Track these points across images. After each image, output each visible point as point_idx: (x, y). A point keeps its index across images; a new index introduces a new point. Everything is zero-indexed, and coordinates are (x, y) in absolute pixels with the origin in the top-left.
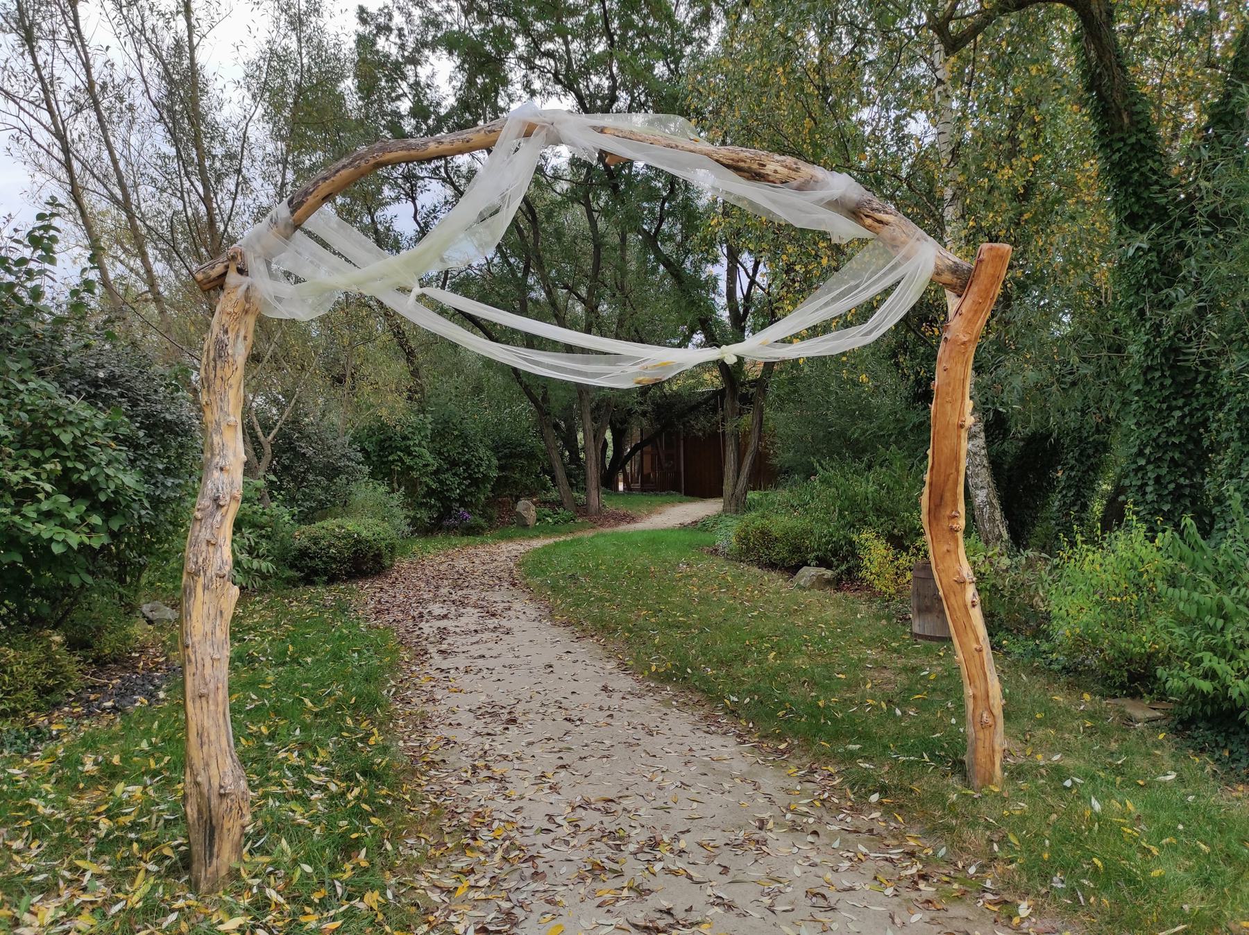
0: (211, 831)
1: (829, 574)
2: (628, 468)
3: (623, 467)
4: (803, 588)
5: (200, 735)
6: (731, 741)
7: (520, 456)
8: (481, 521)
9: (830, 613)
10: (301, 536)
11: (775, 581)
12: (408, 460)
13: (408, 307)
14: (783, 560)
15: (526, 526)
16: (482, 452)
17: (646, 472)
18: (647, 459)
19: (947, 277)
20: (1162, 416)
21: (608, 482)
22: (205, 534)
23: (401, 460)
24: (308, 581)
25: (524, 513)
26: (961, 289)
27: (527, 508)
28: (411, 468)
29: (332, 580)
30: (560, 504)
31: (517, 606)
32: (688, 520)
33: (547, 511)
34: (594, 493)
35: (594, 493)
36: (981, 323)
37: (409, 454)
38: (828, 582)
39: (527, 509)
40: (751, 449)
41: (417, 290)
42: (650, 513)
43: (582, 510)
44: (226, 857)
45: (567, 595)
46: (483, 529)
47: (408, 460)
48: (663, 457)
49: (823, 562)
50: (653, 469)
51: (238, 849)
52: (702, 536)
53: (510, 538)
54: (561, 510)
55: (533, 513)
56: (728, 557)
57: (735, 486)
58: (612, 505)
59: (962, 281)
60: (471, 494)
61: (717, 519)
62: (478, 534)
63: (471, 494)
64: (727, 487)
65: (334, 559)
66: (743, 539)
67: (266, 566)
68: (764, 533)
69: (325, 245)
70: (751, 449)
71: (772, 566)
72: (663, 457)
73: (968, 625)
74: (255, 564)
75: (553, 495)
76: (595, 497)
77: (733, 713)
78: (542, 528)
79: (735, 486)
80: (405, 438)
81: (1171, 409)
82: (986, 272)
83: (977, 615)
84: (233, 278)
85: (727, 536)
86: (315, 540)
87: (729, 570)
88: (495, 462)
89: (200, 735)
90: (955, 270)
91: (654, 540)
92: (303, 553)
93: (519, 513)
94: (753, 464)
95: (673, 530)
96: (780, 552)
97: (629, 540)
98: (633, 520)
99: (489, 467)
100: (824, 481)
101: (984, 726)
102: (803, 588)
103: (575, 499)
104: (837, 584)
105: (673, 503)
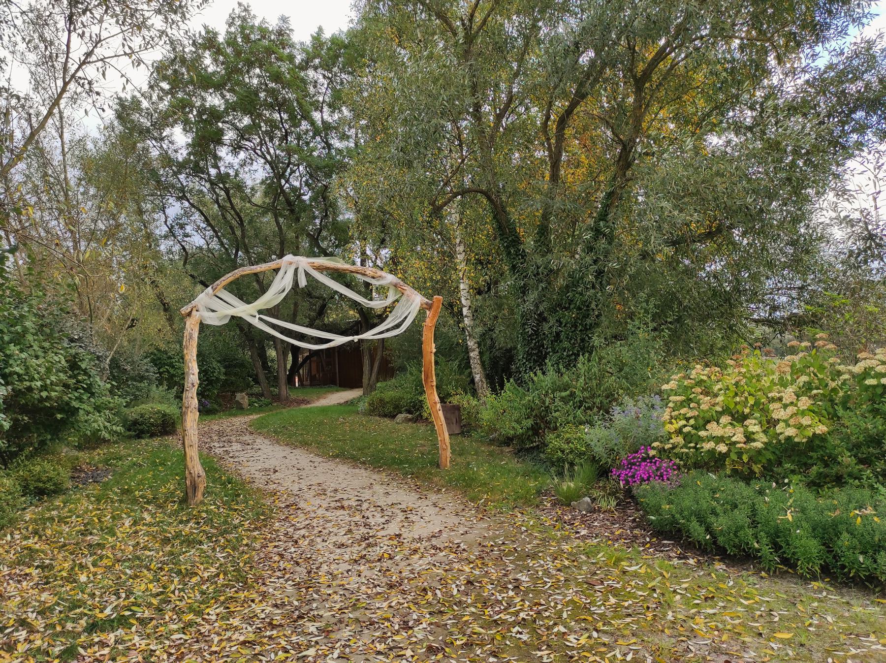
0: (195, 488)
1: (410, 416)
2: (301, 371)
3: (298, 371)
4: (397, 423)
5: (191, 458)
6: (363, 471)
7: (235, 366)
8: (216, 406)
9: (409, 431)
10: (133, 413)
11: (387, 421)
12: (172, 371)
13: (255, 322)
14: (390, 412)
15: (242, 409)
16: (215, 364)
17: (313, 373)
18: (314, 366)
19: (425, 306)
20: (529, 342)
21: (290, 381)
22: (190, 395)
23: (168, 371)
24: (139, 436)
25: (241, 401)
26: (430, 309)
27: (242, 398)
28: (173, 375)
29: (152, 435)
30: (262, 395)
31: (257, 440)
32: (342, 401)
33: (254, 399)
34: (283, 388)
35: (283, 388)
36: (435, 320)
37: (173, 367)
38: (410, 420)
39: (243, 398)
40: (378, 357)
41: (258, 316)
42: (318, 398)
43: (277, 398)
44: (199, 496)
45: (284, 434)
46: (217, 411)
47: (172, 371)
48: (324, 364)
49: (409, 412)
50: (318, 371)
51: (204, 495)
52: (353, 408)
53: (235, 415)
54: (263, 399)
55: (247, 401)
56: (365, 414)
57: (369, 379)
58: (293, 395)
59: (430, 307)
60: (208, 390)
61: (359, 399)
62: (215, 414)
63: (208, 390)
64: (365, 380)
65: (152, 424)
66: (371, 404)
67: (119, 429)
68: (381, 400)
69: (221, 299)
70: (378, 357)
71: (385, 416)
72: (324, 364)
73: (438, 417)
74: (114, 428)
75: (257, 389)
76: (284, 390)
77: (364, 463)
78: (252, 409)
79: (369, 379)
80: (170, 358)
81: (532, 340)
82: (435, 305)
83: (441, 413)
84: (194, 313)
85: (363, 406)
86: (142, 416)
87: (364, 420)
88: (223, 370)
89: (191, 458)
90: (427, 304)
91: (324, 410)
92: (135, 423)
93: (237, 402)
94: (380, 363)
95: (334, 405)
96: (390, 408)
97: (311, 411)
98: (308, 403)
99: (219, 373)
100: (411, 374)
101: (444, 449)
102: (397, 423)
103: (271, 392)
104: (415, 420)
105: (332, 392)
